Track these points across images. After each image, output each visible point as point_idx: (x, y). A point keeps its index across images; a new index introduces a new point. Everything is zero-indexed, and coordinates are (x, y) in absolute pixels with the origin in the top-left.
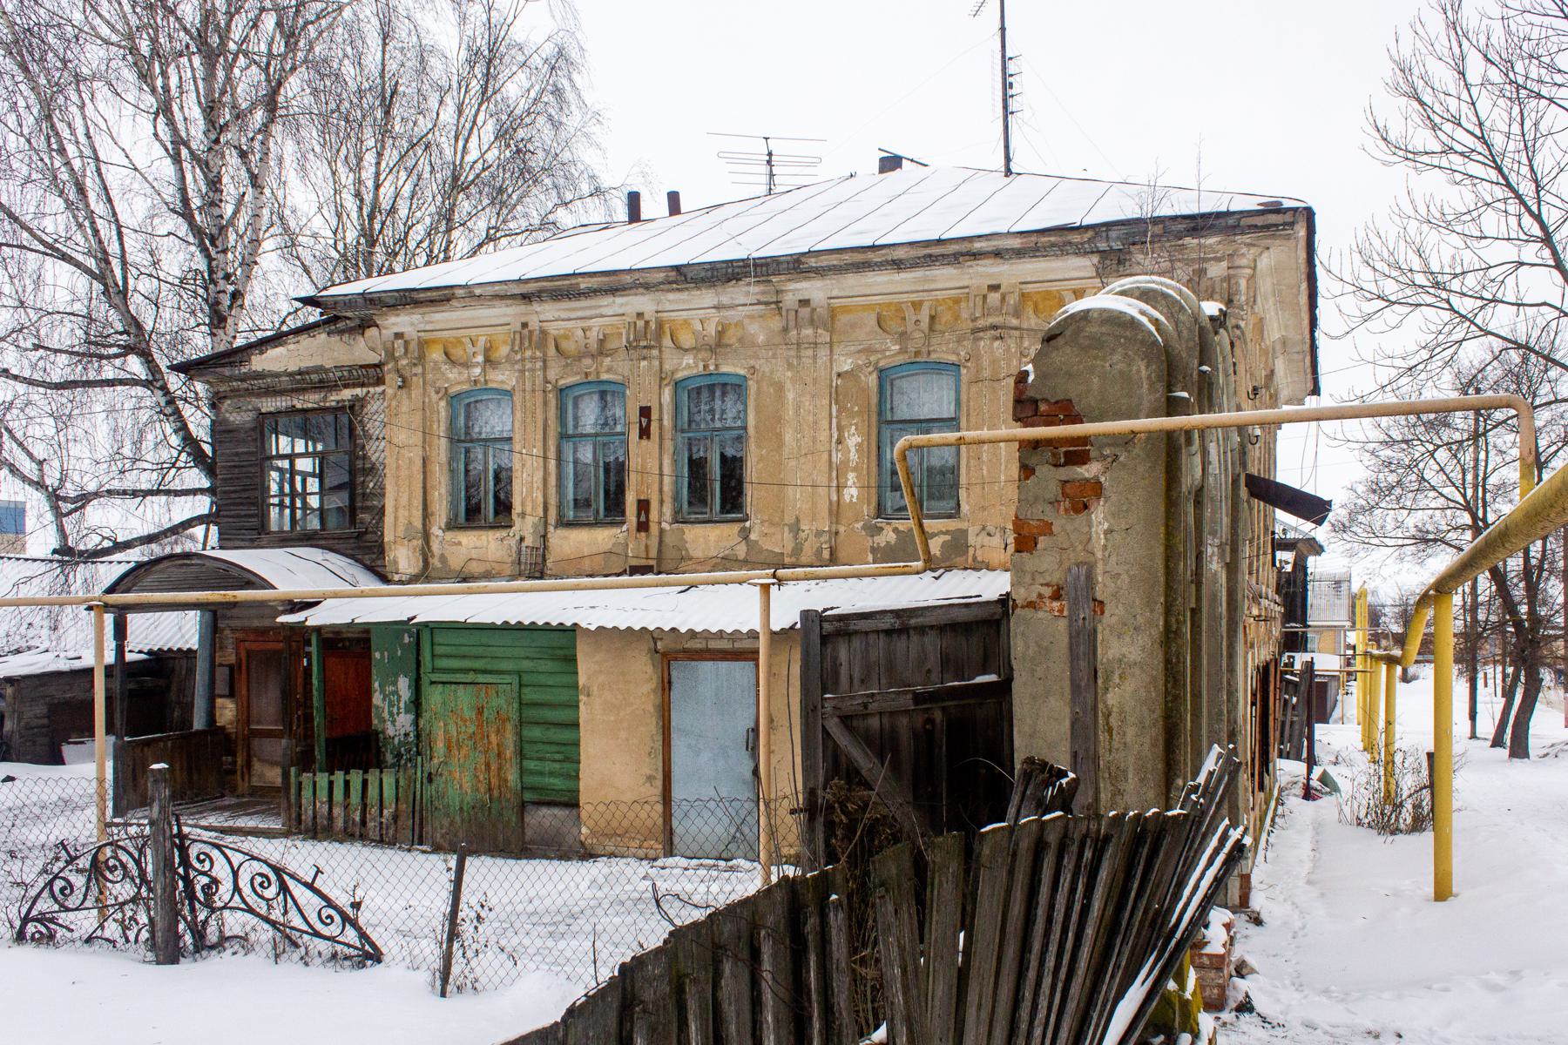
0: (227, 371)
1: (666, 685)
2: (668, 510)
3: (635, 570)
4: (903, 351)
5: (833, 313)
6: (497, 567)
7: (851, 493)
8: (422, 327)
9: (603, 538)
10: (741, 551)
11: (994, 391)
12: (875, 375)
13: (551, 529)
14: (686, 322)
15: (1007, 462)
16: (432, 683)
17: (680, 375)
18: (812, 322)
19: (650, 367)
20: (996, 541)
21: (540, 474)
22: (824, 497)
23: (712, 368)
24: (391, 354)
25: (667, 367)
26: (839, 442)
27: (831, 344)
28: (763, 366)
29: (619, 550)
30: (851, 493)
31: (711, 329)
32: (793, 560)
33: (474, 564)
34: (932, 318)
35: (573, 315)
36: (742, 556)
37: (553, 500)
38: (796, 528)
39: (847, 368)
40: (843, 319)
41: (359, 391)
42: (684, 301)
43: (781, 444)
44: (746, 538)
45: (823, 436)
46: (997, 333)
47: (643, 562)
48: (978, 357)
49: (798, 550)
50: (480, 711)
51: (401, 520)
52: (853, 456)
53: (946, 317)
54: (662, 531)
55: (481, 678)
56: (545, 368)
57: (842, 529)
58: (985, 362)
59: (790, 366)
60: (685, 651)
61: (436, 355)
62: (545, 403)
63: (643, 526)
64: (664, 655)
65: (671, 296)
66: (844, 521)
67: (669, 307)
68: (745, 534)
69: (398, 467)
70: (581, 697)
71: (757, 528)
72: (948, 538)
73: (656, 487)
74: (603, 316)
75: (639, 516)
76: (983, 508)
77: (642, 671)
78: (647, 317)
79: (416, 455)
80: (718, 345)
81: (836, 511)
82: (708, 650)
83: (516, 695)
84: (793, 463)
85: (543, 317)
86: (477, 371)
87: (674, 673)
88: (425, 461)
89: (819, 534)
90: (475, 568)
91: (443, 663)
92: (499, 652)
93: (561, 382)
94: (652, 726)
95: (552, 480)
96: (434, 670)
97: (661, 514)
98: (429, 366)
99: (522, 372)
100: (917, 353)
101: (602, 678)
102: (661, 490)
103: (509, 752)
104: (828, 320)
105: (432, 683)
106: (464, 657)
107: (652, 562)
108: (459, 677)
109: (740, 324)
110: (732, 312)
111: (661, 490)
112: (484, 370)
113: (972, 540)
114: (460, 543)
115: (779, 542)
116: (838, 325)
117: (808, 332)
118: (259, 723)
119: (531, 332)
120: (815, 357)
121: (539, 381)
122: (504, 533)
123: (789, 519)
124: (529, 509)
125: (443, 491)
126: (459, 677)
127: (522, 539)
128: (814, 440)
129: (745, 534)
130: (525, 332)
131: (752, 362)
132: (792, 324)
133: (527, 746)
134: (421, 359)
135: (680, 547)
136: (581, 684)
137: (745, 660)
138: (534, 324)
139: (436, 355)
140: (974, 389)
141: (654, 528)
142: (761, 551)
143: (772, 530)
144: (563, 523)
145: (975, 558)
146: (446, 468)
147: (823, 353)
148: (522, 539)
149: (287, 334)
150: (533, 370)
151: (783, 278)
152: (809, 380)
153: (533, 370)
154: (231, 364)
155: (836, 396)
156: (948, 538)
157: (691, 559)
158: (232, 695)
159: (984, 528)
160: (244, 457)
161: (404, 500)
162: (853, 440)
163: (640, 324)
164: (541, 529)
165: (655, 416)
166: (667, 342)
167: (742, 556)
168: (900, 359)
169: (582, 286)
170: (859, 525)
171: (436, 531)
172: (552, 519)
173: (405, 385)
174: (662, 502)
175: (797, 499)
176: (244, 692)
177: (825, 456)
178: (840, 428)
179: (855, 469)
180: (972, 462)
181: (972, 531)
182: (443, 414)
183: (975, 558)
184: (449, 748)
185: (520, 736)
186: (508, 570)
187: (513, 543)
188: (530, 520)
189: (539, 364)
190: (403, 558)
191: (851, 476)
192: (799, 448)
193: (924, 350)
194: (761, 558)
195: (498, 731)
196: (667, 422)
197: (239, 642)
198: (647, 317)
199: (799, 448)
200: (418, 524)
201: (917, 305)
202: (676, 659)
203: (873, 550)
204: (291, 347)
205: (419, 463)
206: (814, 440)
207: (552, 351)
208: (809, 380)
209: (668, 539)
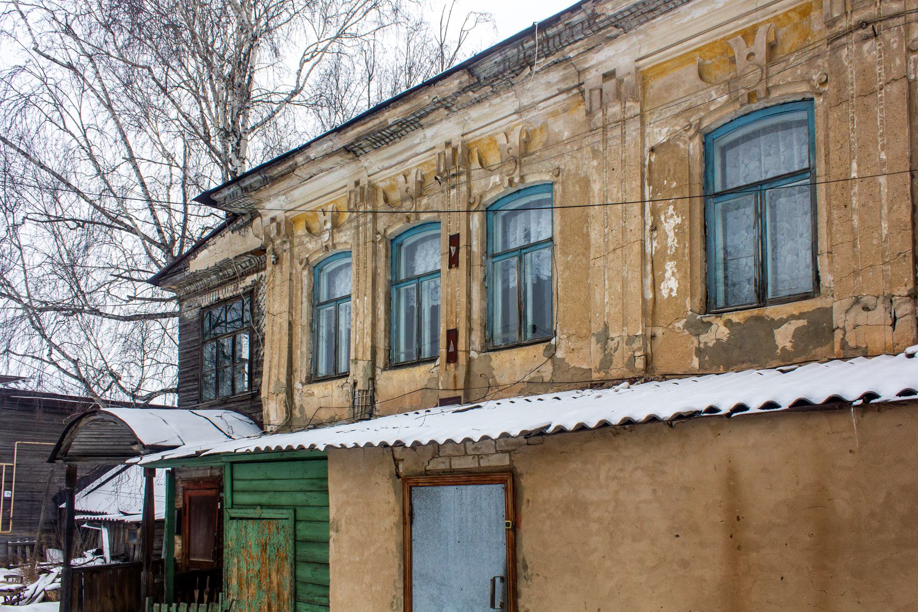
0: (178, 277)
1: (408, 518)
2: (477, 338)
3: (444, 402)
4: (733, 100)
5: (643, 77)
6: (338, 412)
7: (671, 285)
8: (287, 207)
9: (420, 374)
10: (547, 372)
11: (867, 108)
12: (697, 140)
13: (378, 371)
14: (492, 139)
15: (891, 202)
16: (232, 518)
17: (489, 198)
18: (618, 96)
19: (458, 194)
20: (879, 315)
21: (369, 320)
22: (636, 289)
23: (516, 180)
24: (267, 236)
25: (475, 192)
26: (654, 228)
27: (642, 115)
28: (567, 163)
29: (433, 385)
30: (671, 285)
31: (515, 139)
32: (602, 374)
33: (323, 412)
34: (772, 47)
35: (393, 162)
36: (547, 376)
37: (382, 344)
38: (604, 337)
39: (662, 139)
40: (656, 84)
41: (255, 277)
42: (486, 116)
43: (587, 247)
44: (552, 357)
45: (634, 224)
46: (868, 31)
47: (451, 394)
48: (839, 71)
49: (606, 363)
50: (264, 548)
51: (273, 378)
52: (672, 241)
53: (790, 40)
54: (470, 361)
55: (267, 513)
56: (375, 220)
57: (659, 332)
58: (851, 75)
59: (595, 153)
60: (426, 473)
61: (300, 231)
62: (375, 253)
63: (452, 357)
64: (405, 480)
65: (475, 112)
66: (662, 322)
67: (474, 126)
68: (551, 354)
69: (273, 333)
70: (332, 533)
71: (563, 344)
72: (802, 323)
73: (463, 315)
74: (418, 155)
75: (448, 348)
76: (856, 273)
77: (385, 498)
78: (454, 144)
79: (283, 320)
80: (522, 155)
81: (651, 311)
82: (452, 472)
83: (291, 531)
84: (600, 263)
85: (370, 172)
86: (326, 236)
87: (416, 502)
88: (291, 325)
89: (631, 339)
90: (324, 415)
91: (240, 498)
92: (278, 485)
93: (390, 231)
94: (394, 571)
95: (381, 325)
96: (233, 506)
97: (469, 342)
98: (296, 241)
99: (357, 227)
100: (752, 96)
101: (349, 510)
102: (469, 318)
103: (286, 594)
104: (637, 87)
105: (232, 518)
106: (255, 491)
107: (460, 393)
108: (251, 513)
109: (544, 127)
110: (534, 113)
111: (469, 318)
112: (332, 235)
113: (838, 319)
114: (313, 394)
115: (587, 357)
116: (651, 93)
117: (615, 109)
118: (194, 556)
119: (362, 188)
120: (623, 135)
121: (370, 233)
122: (343, 380)
123: (596, 327)
124: (360, 356)
125: (304, 349)
126: (251, 513)
127: (355, 384)
128: (624, 231)
129: (551, 354)
130: (358, 189)
131: (557, 163)
132: (596, 104)
133: (300, 586)
134: (290, 235)
135: (488, 376)
136: (331, 518)
137: (492, 482)
138: (364, 182)
139: (300, 231)
140: (834, 115)
141: (462, 357)
142: (568, 369)
143: (580, 344)
144: (393, 365)
145: (844, 344)
146: (307, 329)
147: (633, 129)
148: (355, 384)
149: (208, 238)
150: (365, 224)
151: (580, 46)
152: (616, 164)
153: (365, 224)
154: (180, 271)
155: (648, 175)
156: (802, 323)
157: (497, 386)
158: (179, 533)
159: (857, 301)
160: (193, 345)
161: (275, 361)
162: (671, 222)
163: (449, 152)
164: (369, 372)
165: (463, 242)
166: (476, 164)
167: (547, 376)
168: (730, 112)
169: (390, 122)
170: (680, 324)
171: (297, 385)
172: (380, 362)
173: (277, 260)
174: (470, 330)
175: (605, 299)
176: (187, 531)
177: (637, 247)
178: (655, 213)
179: (674, 257)
180: (835, 214)
181: (838, 307)
182: (306, 281)
183: (844, 344)
184: (240, 584)
185: (294, 575)
186: (347, 413)
187: (348, 388)
188: (361, 364)
189: (370, 216)
190: (274, 411)
191: (670, 266)
192: (607, 243)
193: (761, 88)
194: (568, 377)
195: (278, 571)
196: (476, 247)
197: (185, 489)
198: (454, 144)
199: (607, 243)
200: (283, 380)
201: (748, 35)
202: (417, 485)
203: (699, 352)
204: (211, 248)
205: (286, 326)
206: (624, 231)
207: (381, 202)
208: (616, 164)
209: (476, 369)
